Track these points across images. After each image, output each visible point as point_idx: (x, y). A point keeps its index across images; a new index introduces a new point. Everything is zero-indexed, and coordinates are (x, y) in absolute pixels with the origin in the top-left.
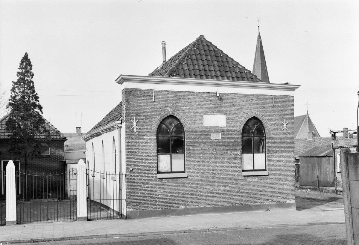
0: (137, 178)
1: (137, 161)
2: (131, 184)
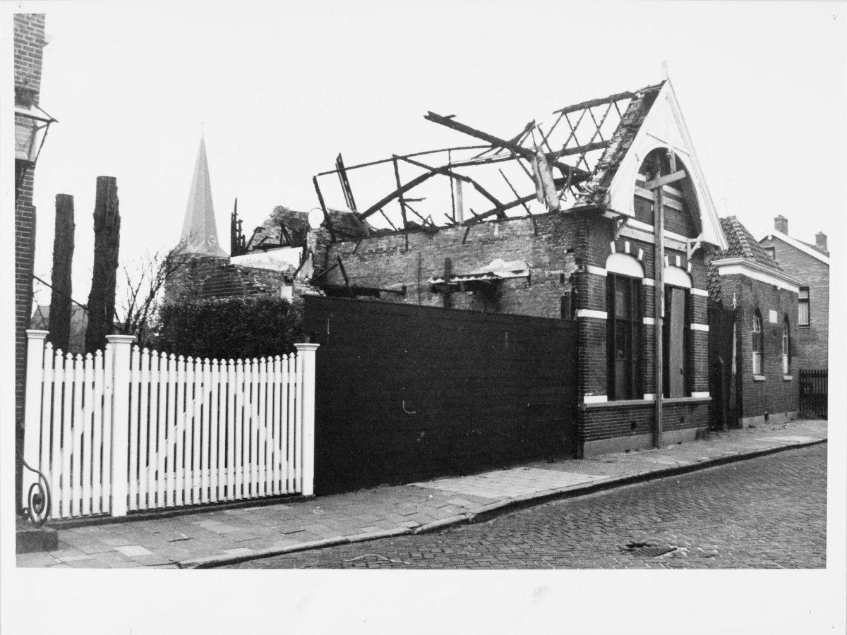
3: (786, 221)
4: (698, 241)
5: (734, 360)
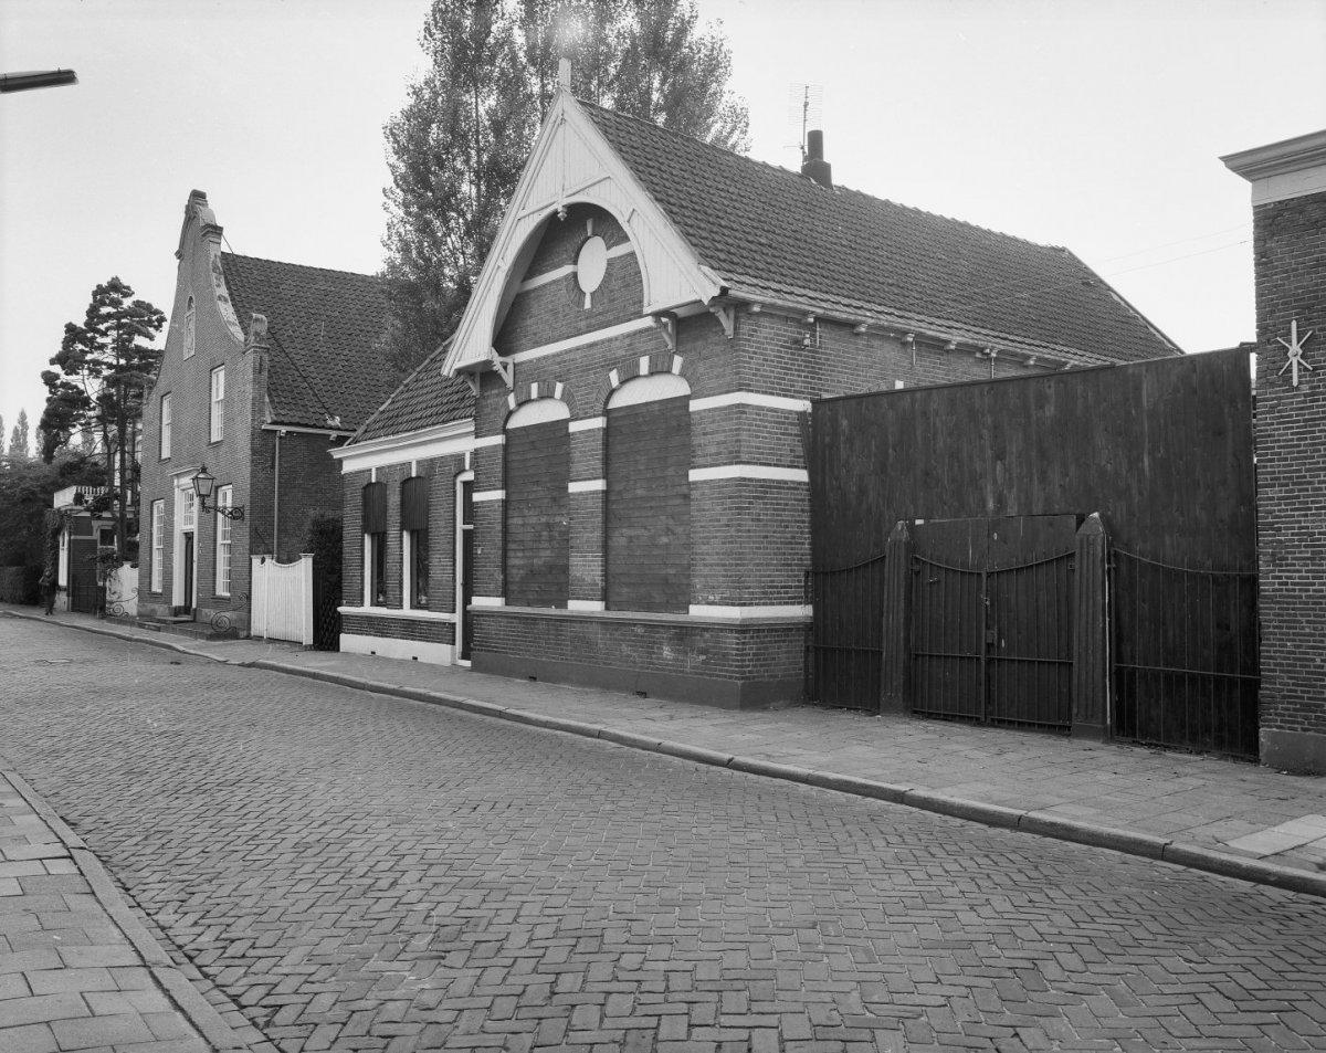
0: (1308, 591)
1: (1306, 515)
2: (1279, 615)
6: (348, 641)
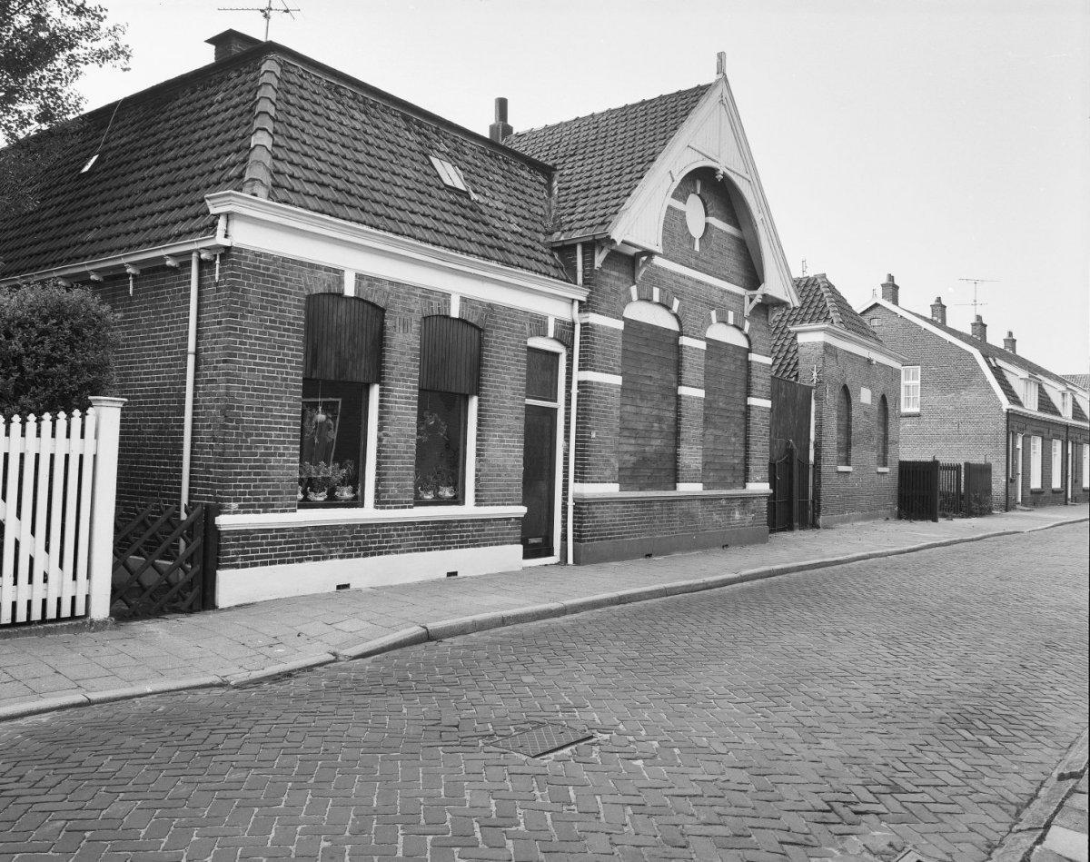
3: (945, 307)
4: (759, 293)
5: (812, 446)
6: (232, 585)
